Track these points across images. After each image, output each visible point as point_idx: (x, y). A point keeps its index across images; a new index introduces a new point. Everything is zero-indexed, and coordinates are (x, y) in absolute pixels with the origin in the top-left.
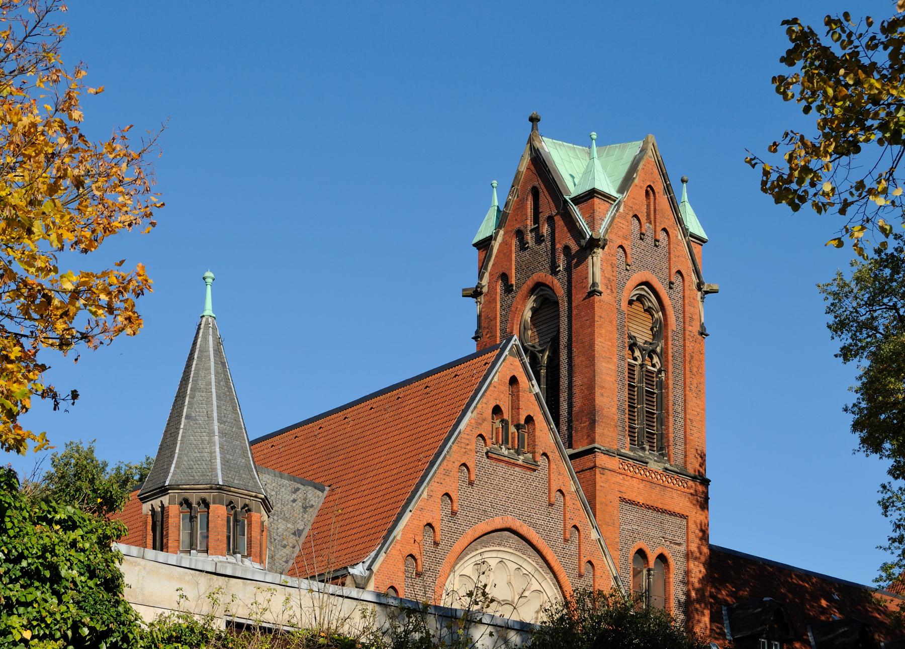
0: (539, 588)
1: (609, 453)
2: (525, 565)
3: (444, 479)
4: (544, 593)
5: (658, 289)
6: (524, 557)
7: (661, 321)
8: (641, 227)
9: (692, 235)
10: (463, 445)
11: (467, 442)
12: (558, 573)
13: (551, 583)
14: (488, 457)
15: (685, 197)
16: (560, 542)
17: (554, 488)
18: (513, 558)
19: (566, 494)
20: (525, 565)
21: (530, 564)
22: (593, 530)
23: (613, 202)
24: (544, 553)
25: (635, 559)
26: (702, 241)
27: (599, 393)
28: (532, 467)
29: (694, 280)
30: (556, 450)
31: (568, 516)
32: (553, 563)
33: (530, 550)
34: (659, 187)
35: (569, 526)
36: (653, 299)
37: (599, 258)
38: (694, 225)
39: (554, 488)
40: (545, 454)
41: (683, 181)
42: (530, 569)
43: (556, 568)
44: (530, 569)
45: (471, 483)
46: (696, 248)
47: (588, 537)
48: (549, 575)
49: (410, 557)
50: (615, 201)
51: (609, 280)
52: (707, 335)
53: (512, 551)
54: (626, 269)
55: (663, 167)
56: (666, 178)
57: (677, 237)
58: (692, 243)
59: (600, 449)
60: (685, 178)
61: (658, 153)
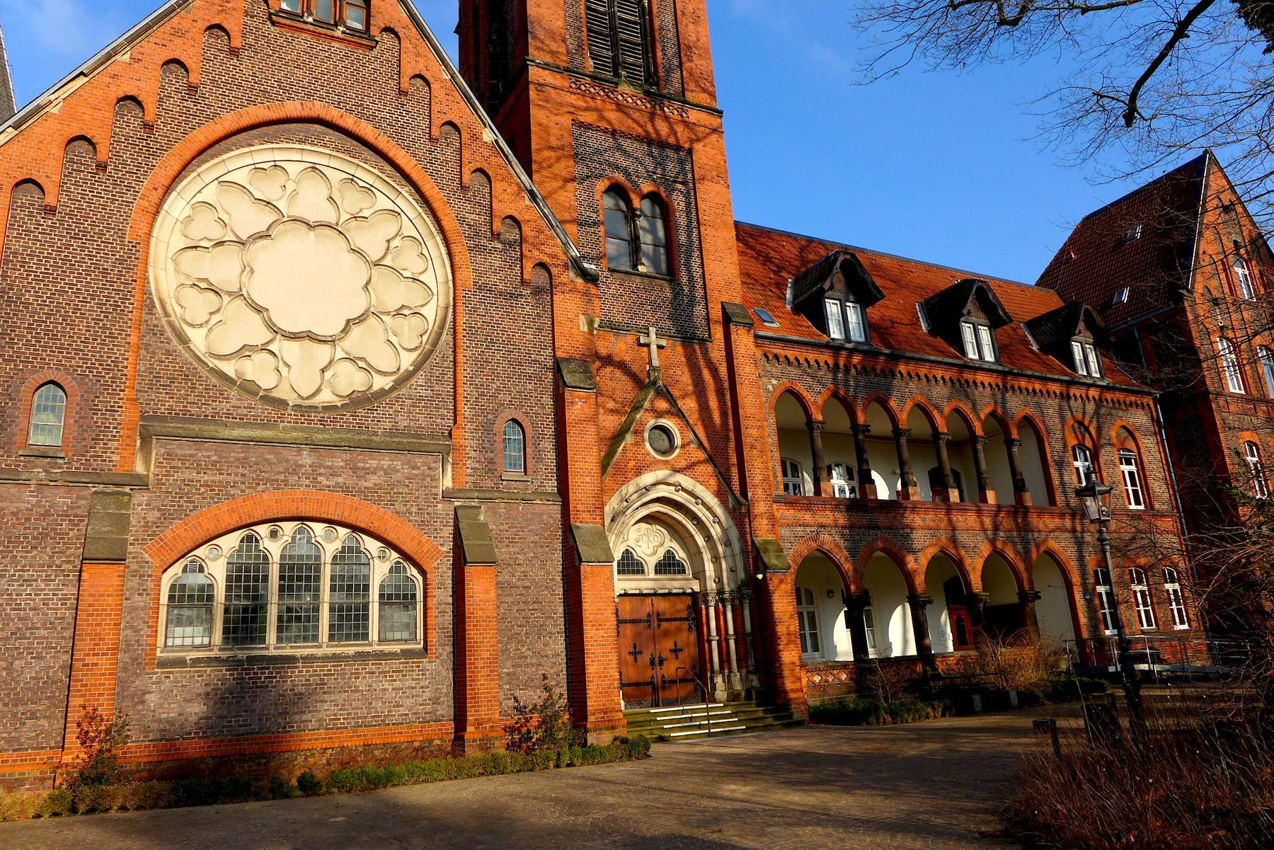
2: (360, 173)
6: (355, 161)
13: (410, 199)
14: (273, 23)
16: (424, 145)
17: (408, 71)
18: (334, 163)
19: (431, 80)
20: (360, 173)
21: (368, 173)
24: (391, 154)
25: (757, 346)
30: (411, 26)
31: (435, 108)
33: (367, 153)
35: (437, 122)
39: (408, 71)
40: (388, 29)
43: (415, 176)
44: (370, 179)
47: (476, 137)
49: (657, 431)
53: (330, 152)
59: (533, 61)
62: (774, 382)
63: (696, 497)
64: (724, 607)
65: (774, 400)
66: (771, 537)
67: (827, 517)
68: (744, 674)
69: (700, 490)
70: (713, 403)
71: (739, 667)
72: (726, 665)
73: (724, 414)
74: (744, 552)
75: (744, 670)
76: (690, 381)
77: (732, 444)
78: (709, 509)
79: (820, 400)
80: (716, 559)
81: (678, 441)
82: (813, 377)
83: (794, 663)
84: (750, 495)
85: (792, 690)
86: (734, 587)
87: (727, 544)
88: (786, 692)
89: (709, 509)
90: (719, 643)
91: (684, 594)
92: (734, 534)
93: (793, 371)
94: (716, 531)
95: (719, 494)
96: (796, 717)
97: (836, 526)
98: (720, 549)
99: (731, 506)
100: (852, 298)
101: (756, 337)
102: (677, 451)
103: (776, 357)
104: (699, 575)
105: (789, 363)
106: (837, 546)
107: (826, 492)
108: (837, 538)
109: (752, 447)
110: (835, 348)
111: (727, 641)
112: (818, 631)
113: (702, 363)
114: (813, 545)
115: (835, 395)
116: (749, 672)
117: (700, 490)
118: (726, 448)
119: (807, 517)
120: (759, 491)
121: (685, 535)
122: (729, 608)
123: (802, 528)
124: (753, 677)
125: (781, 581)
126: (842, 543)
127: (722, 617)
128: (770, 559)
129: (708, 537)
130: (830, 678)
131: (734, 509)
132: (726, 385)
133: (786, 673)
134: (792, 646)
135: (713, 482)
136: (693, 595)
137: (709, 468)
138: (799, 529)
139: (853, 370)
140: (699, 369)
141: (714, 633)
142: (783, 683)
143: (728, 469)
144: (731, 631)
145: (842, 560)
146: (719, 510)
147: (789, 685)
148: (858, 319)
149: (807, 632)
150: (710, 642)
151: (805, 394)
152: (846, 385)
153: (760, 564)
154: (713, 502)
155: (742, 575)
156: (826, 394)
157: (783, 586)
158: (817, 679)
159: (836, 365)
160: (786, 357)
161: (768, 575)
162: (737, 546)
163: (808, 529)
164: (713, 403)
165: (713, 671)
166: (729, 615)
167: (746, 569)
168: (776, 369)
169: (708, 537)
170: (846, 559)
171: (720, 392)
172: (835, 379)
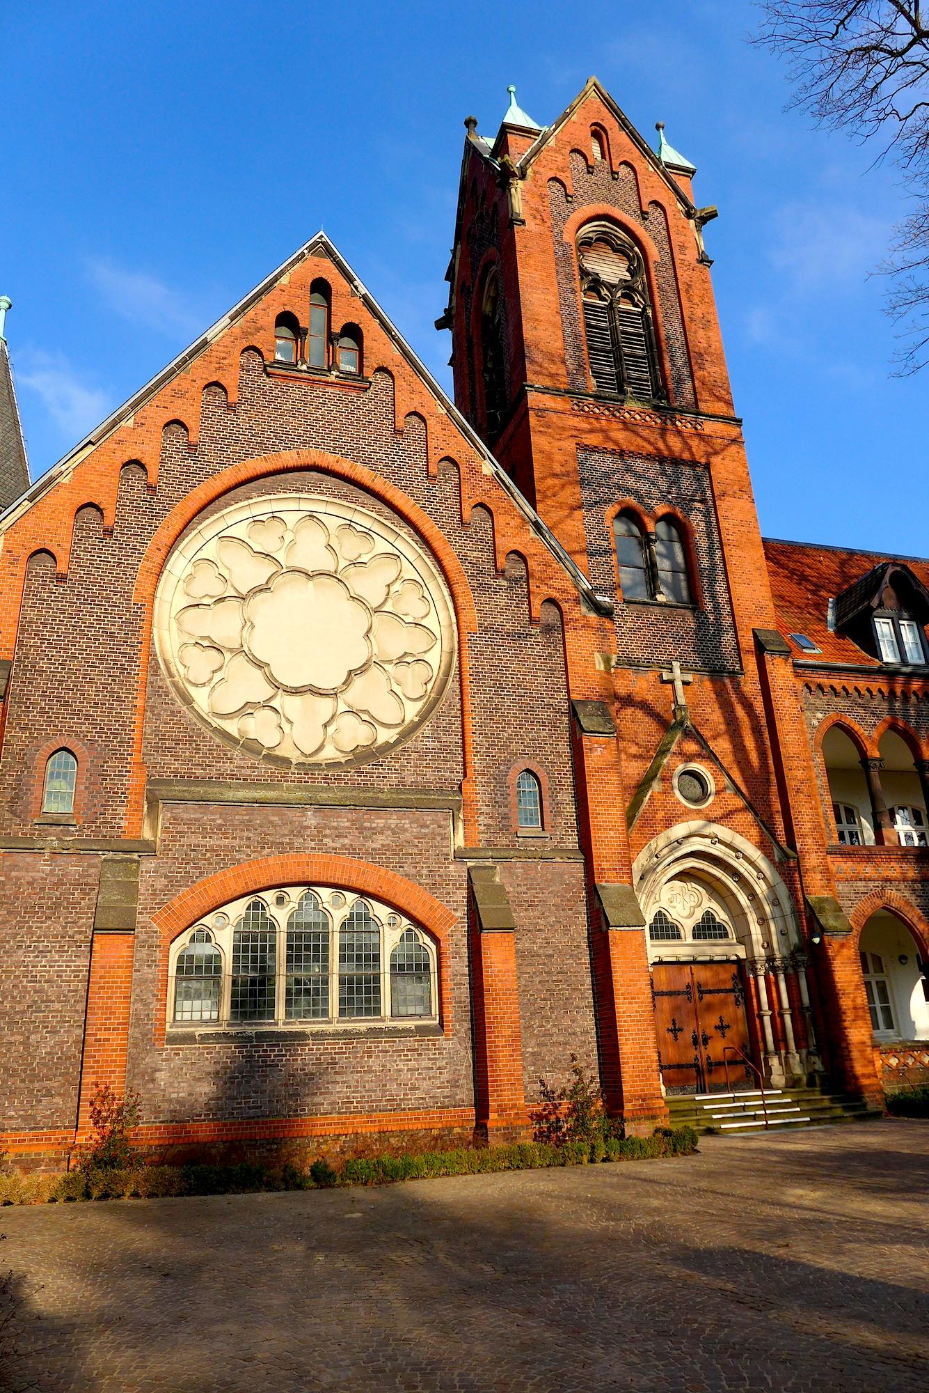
0: (390, 549)
1: (550, 391)
2: (357, 518)
3: (171, 402)
4: (402, 556)
5: (619, 218)
7: (638, 256)
8: (586, 160)
9: (669, 166)
10: (213, 359)
11: (224, 355)
12: (419, 523)
13: (409, 540)
14: (268, 375)
15: (663, 140)
17: (403, 409)
18: (331, 509)
20: (357, 518)
21: (408, 546)
22: (485, 462)
23: (536, 137)
24: (388, 496)
26: (690, 173)
27: (529, 326)
28: (358, 381)
29: (681, 208)
30: (404, 363)
31: (432, 444)
32: (406, 509)
33: (364, 497)
34: (610, 123)
35: (434, 459)
36: (622, 234)
37: (519, 190)
38: (669, 155)
39: (403, 409)
41: (658, 127)
42: (367, 523)
43: (413, 515)
44: (367, 523)
45: (231, 407)
46: (682, 183)
47: (475, 471)
48: (405, 530)
50: (538, 135)
51: (536, 210)
52: (711, 262)
53: (326, 499)
54: (568, 201)
55: (612, 102)
56: (642, 142)
57: (647, 169)
58: (672, 176)
60: (661, 123)
61: (603, 91)
62: (820, 715)
63: (736, 850)
64: (776, 976)
65: (820, 737)
66: (826, 894)
67: (893, 869)
68: (804, 1056)
69: (740, 841)
70: (750, 743)
71: (798, 1047)
72: (782, 1045)
73: (762, 755)
74: (796, 912)
75: (804, 1051)
76: (721, 720)
77: (774, 789)
78: (752, 863)
79: (875, 734)
80: (763, 921)
81: (712, 787)
82: (865, 709)
83: (864, 1043)
84: (798, 846)
85: (863, 1075)
86: (786, 953)
87: (775, 903)
88: (856, 1078)
89: (752, 863)
90: (772, 1018)
91: (728, 961)
92: (783, 891)
93: (841, 703)
94: (761, 888)
95: (762, 846)
96: (871, 1107)
97: (904, 880)
98: (767, 909)
99: (777, 860)
100: (905, 615)
101: (795, 665)
102: (711, 799)
103: (820, 687)
104: (744, 939)
105: (836, 694)
106: (908, 903)
107: (890, 840)
108: (907, 894)
109: (798, 791)
110: (890, 674)
111: (781, 1016)
112: (891, 1005)
113: (734, 698)
114: (879, 902)
115: (893, 727)
116: (809, 1053)
117: (740, 841)
118: (768, 793)
119: (869, 870)
120: (809, 841)
121: (726, 893)
122: (782, 977)
123: (864, 883)
124: (815, 1059)
125: (842, 946)
126: (913, 900)
127: (774, 989)
128: (828, 920)
129: (753, 896)
130: (910, 1061)
131: (781, 862)
132: (764, 722)
133: (855, 1054)
134: (860, 1023)
135: (754, 832)
136: (739, 962)
137: (749, 817)
138: (860, 884)
139: (913, 698)
140: (731, 705)
141: (765, 1006)
142: (852, 1067)
143: (771, 817)
144: (786, 1004)
145: (915, 920)
146: (763, 864)
147: (859, 1069)
148: (914, 637)
149: (878, 1005)
150: (761, 1017)
151: (856, 727)
152: (906, 716)
153: (816, 926)
154: (756, 854)
155: (794, 939)
156: (882, 727)
157: (845, 952)
158: (894, 1062)
159: (892, 693)
160: (831, 687)
161: (826, 939)
162: (787, 905)
163: (871, 884)
164: (750, 743)
165: (766, 1052)
166: (783, 986)
167: (799, 932)
168: (820, 701)
169: (753, 896)
170: (920, 918)
171: (756, 730)
172: (891, 709)
